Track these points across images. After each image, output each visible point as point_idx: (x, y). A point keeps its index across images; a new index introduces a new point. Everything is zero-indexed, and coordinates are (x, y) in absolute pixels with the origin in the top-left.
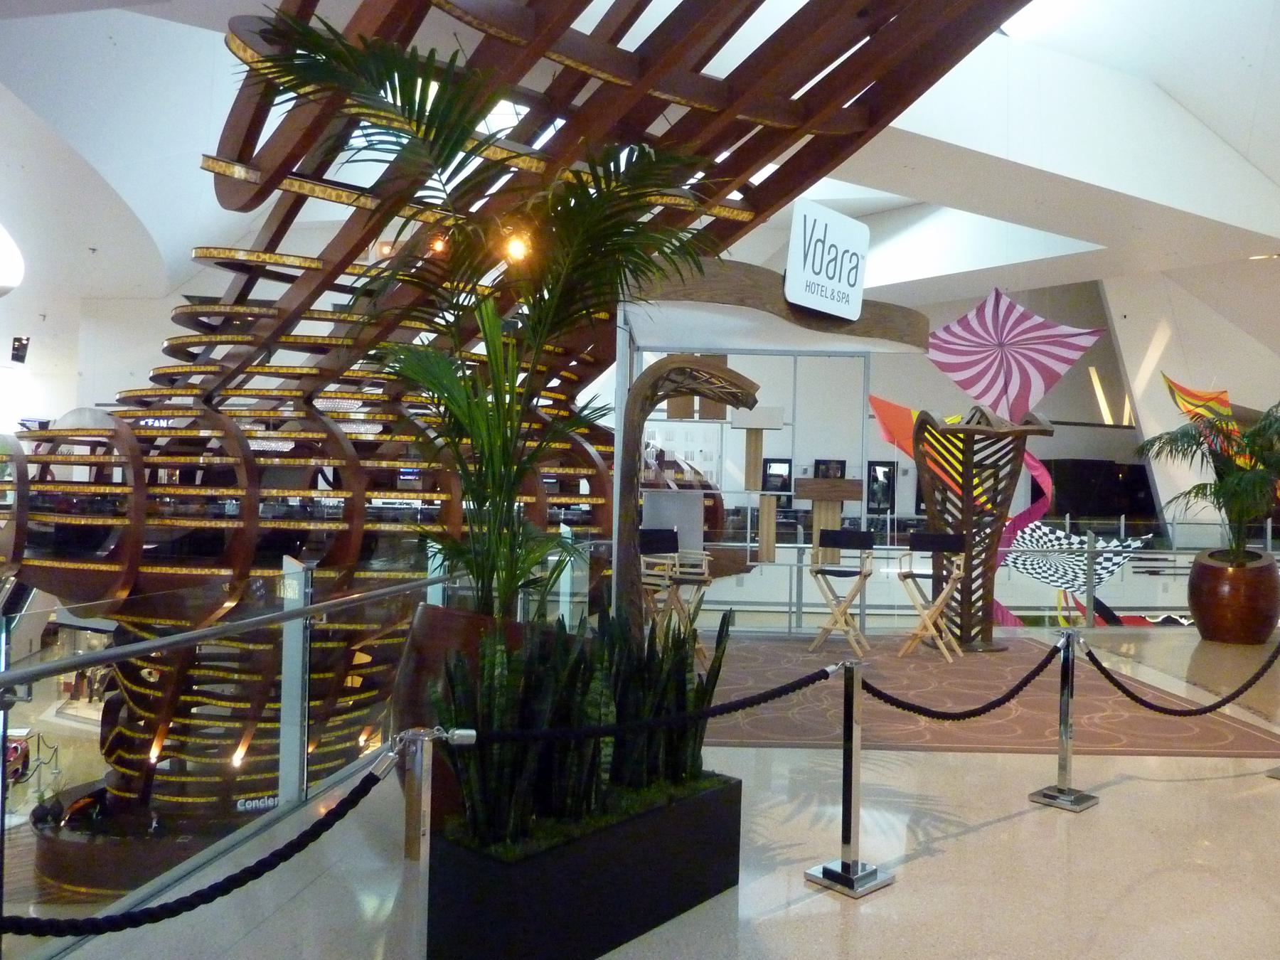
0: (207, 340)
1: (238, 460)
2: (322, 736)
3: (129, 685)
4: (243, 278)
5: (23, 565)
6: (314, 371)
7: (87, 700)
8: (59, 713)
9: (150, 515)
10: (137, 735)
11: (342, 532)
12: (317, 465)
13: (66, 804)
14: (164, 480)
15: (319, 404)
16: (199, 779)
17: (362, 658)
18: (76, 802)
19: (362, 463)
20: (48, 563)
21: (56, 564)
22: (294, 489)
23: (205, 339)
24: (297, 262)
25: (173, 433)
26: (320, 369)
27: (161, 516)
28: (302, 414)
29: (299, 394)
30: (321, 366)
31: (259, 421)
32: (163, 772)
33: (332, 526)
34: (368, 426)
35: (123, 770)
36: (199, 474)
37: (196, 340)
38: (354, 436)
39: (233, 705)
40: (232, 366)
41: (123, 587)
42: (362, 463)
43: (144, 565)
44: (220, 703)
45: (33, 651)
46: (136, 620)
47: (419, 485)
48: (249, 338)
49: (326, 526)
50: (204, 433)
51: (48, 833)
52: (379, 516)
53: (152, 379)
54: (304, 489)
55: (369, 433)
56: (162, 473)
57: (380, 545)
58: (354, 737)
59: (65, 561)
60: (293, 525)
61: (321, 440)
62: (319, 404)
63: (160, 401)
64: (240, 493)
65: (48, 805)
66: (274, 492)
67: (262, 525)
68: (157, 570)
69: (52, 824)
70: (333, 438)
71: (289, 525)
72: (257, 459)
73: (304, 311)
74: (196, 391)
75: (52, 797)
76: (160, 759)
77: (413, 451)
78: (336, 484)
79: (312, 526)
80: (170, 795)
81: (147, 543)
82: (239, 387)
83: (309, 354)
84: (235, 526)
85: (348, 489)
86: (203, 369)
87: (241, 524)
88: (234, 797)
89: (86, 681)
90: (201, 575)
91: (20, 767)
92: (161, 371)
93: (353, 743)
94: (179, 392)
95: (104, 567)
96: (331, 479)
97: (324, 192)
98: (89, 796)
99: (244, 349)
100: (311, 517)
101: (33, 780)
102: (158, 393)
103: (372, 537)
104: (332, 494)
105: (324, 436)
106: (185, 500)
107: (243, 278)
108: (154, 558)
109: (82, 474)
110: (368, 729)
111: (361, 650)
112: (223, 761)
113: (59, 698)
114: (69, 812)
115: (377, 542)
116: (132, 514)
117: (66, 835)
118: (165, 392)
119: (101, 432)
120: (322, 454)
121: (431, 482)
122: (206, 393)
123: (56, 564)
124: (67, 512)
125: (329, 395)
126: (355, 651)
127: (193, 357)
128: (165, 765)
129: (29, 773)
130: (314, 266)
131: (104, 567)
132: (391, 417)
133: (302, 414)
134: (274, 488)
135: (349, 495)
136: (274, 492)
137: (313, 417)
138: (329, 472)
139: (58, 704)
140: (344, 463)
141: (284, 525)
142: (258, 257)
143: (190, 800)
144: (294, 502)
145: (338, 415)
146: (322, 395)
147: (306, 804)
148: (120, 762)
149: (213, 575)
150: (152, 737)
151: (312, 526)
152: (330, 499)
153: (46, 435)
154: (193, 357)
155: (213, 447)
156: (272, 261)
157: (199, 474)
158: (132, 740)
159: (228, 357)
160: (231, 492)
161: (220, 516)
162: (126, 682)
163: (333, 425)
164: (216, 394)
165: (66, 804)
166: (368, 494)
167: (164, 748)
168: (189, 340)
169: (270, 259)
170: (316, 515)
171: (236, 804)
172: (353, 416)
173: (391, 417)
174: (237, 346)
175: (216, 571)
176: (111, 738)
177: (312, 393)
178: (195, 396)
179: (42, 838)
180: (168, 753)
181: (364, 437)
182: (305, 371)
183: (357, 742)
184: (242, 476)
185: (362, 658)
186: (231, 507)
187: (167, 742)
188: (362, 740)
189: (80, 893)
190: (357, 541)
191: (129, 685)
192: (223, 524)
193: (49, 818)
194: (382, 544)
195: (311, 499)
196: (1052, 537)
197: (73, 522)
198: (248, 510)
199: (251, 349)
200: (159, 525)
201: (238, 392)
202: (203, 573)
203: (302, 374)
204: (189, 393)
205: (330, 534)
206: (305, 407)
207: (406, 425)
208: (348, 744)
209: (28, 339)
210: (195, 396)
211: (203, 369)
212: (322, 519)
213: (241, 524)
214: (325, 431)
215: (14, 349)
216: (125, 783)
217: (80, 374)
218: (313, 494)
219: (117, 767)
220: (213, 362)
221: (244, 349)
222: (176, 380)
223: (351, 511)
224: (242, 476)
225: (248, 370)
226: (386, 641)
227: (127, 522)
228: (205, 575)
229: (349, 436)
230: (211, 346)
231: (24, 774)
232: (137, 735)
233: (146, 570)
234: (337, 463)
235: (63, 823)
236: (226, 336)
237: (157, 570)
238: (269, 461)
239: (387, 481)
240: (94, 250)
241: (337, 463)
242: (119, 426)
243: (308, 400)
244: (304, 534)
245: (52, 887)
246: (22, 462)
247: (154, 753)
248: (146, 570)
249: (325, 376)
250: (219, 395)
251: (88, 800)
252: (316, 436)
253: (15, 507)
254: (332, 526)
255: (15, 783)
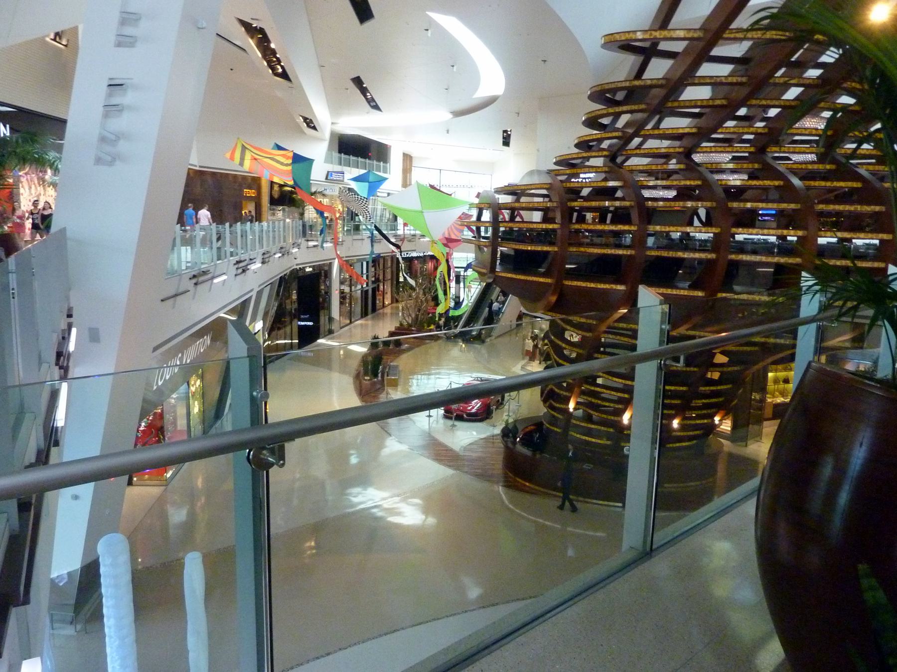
0: (613, 111)
1: (633, 203)
2: (687, 413)
3: (558, 359)
4: (640, 59)
5: (496, 276)
6: (694, 130)
7: (538, 362)
8: (523, 368)
9: (571, 245)
10: (562, 392)
11: (709, 261)
12: (692, 206)
13: (520, 428)
14: (590, 221)
15: (697, 158)
16: (599, 427)
17: (720, 359)
18: (527, 427)
19: (730, 204)
20: (509, 275)
21: (514, 276)
22: (674, 226)
23: (611, 110)
24: (681, 34)
25: (595, 184)
26: (699, 128)
27: (581, 245)
28: (682, 166)
29: (681, 150)
30: (699, 126)
31: (650, 173)
32: (578, 419)
33: (703, 256)
34: (736, 176)
35: (553, 412)
36: (609, 216)
37: (605, 112)
38: (724, 182)
39: (623, 381)
40: (630, 131)
41: (553, 294)
42: (730, 204)
43: (566, 280)
44: (615, 379)
45: (513, 328)
46: (564, 316)
47: (774, 225)
48: (643, 106)
49: (697, 255)
50: (611, 184)
51: (510, 445)
52: (742, 248)
53: (577, 146)
54: (681, 225)
55: (735, 180)
56: (589, 216)
57: (740, 272)
58: (712, 417)
59: (519, 274)
60: (671, 254)
61: (697, 186)
62: (697, 158)
63: (582, 163)
64: (633, 228)
65: (510, 427)
66: (658, 228)
67: (648, 253)
68: (575, 283)
69: (512, 439)
70: (707, 185)
71: (668, 254)
72: (646, 203)
73: (688, 78)
74: (605, 153)
75: (512, 422)
76: (575, 409)
77: (774, 195)
78: (708, 223)
79: (686, 255)
80: (581, 434)
81: (571, 264)
82: (639, 147)
83: (690, 119)
84: (629, 253)
85: (715, 226)
86: (610, 135)
87: (633, 252)
88: (623, 444)
89: (538, 350)
90: (603, 289)
91: (500, 399)
92: (582, 140)
93: (710, 421)
94: (594, 154)
95: (541, 280)
96: (704, 219)
97: (721, 80)
98: (533, 425)
99: (639, 116)
100: (686, 249)
101: (506, 407)
102: (580, 156)
103: (735, 266)
104: (704, 229)
105: (699, 183)
106: (600, 234)
107: (640, 59)
108: (573, 275)
109: (537, 216)
110: (722, 412)
111: (722, 353)
112: (619, 419)
113: (523, 359)
114: (523, 433)
115: (737, 270)
116: (559, 244)
117: (520, 448)
118: (585, 155)
119: (542, 186)
120: (698, 199)
121: (785, 220)
122: (613, 153)
123: (514, 276)
124: (522, 242)
125: (705, 150)
126: (715, 354)
127: (603, 127)
128: (580, 412)
129: (505, 403)
130: (696, 35)
131: (541, 280)
132: (756, 166)
133: (682, 166)
134: (659, 225)
135: (717, 230)
136: (658, 228)
137: (692, 168)
138: (702, 213)
139: (523, 362)
140: (714, 204)
141: (665, 254)
142: (651, 35)
143: (594, 440)
144: (676, 235)
145: (712, 166)
146: (699, 150)
147: (651, 557)
148: (551, 407)
149: (612, 289)
150: (570, 395)
151: (686, 255)
152: (703, 235)
153: (514, 191)
154: (603, 127)
155: (619, 196)
156: (662, 37)
157: (609, 216)
158: (559, 395)
159: (628, 125)
160: (626, 228)
161: (619, 246)
162: (555, 357)
163: (709, 176)
164: (619, 154)
165: (520, 428)
166: (734, 230)
167: (578, 403)
168: (599, 113)
169: (660, 35)
170: (691, 246)
171: (623, 449)
172: (724, 166)
173: (756, 166)
174: (635, 114)
175: (614, 286)
176: (546, 392)
177: (692, 148)
178: (605, 156)
179: (507, 447)
180: (580, 407)
181: (732, 183)
182: (687, 130)
183: (713, 420)
184: (635, 216)
185: (720, 359)
186: (628, 239)
187: (579, 400)
188: (717, 419)
189: (525, 485)
190: (721, 269)
191: (558, 359)
192: (620, 252)
193: (511, 435)
194: (742, 272)
195: (688, 234)
196: (354, 196)
197: (523, 248)
198: (639, 242)
199: (645, 115)
200: (576, 251)
201: (638, 151)
202: (605, 287)
203: (684, 133)
204: (600, 155)
205: (700, 261)
206: (685, 160)
207: (768, 171)
208: (706, 421)
209: (511, 131)
210: (605, 156)
211: (610, 135)
212: (695, 250)
213: (633, 252)
214: (699, 179)
215: (504, 138)
216: (553, 421)
217: (538, 150)
218: (688, 229)
219: (549, 410)
220: (618, 130)
221: (639, 116)
222: (592, 146)
223: (719, 244)
224: (635, 216)
225: (642, 133)
226: (741, 348)
227: (556, 249)
228: (606, 289)
229: (720, 183)
230: (617, 116)
231: (502, 404)
232: (562, 392)
233: (568, 283)
234: (708, 204)
235: (518, 439)
236: (626, 107)
237: (575, 283)
238: (655, 204)
239: (749, 220)
240: (545, 61)
241: (708, 204)
242: (554, 181)
243: (687, 155)
244: (680, 262)
245: (511, 478)
246: (496, 209)
247: (572, 405)
248: (568, 283)
249: (702, 135)
250: (622, 155)
251: (532, 427)
252: (693, 183)
253: (491, 237)
254: (703, 256)
255: (497, 408)
